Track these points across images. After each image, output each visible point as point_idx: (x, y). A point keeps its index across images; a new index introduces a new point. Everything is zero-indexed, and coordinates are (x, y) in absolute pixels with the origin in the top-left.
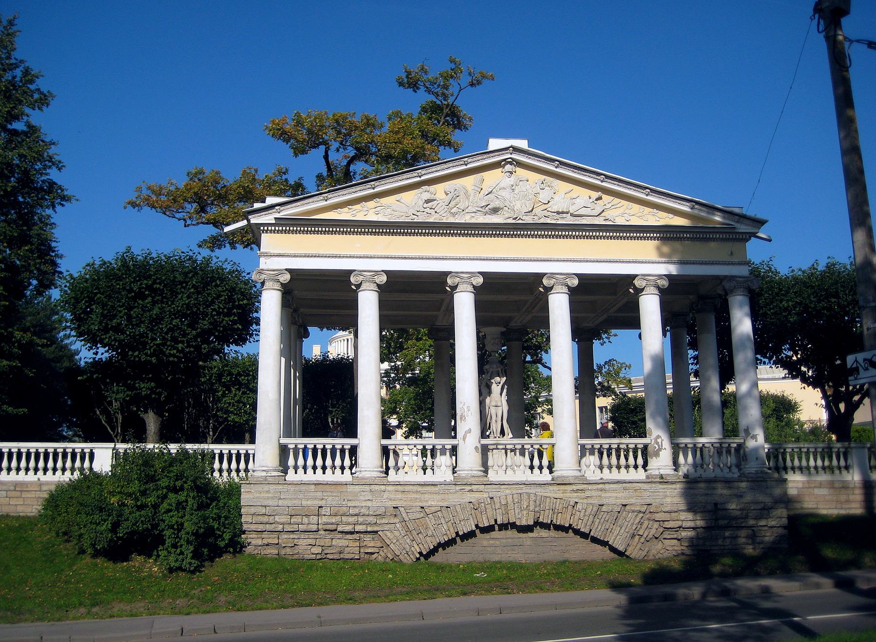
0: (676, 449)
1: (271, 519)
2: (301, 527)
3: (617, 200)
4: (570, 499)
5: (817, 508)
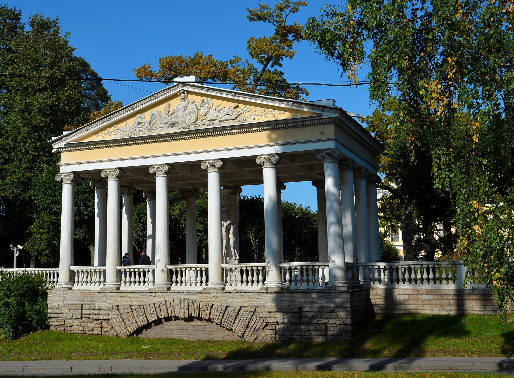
1: (60, 311)
2: (74, 316)
3: (248, 106)
4: (209, 302)
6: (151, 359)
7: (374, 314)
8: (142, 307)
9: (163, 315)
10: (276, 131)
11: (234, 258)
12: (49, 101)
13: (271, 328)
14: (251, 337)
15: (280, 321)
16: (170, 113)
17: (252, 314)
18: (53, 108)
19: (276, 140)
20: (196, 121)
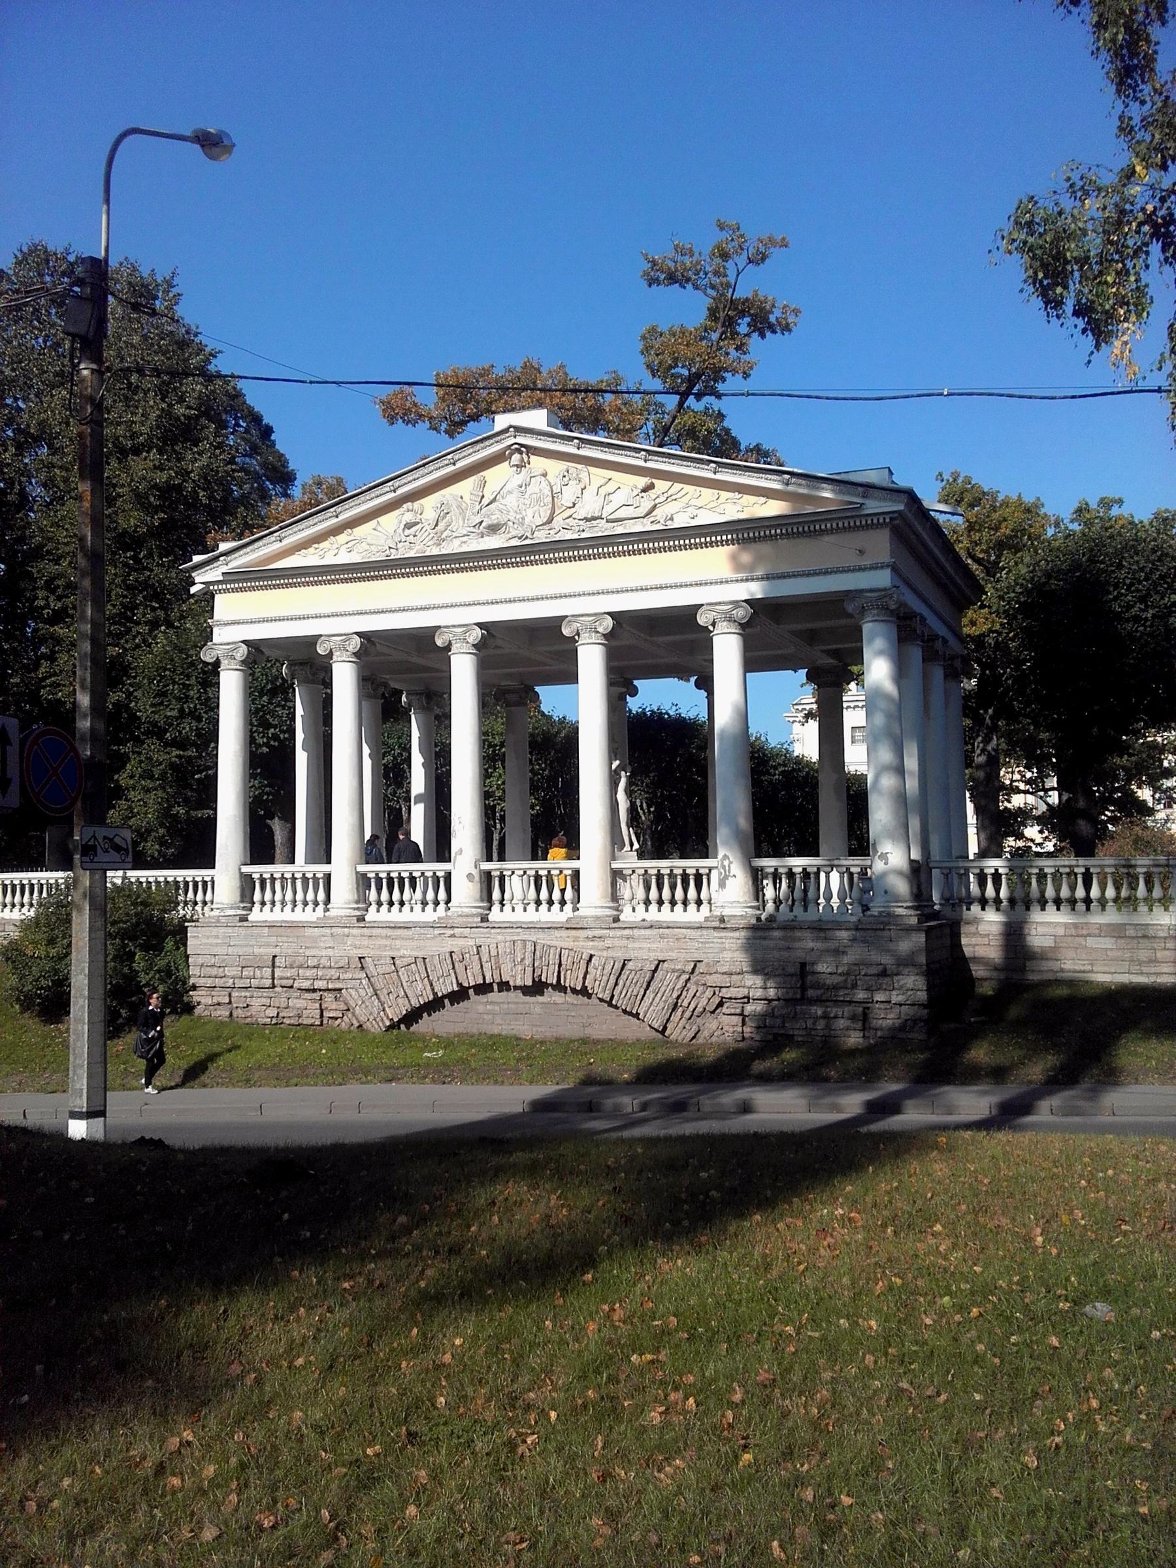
0: (757, 877)
2: (254, 982)
5: (1091, 971)
6: (449, 1082)
7: (971, 981)
8: (420, 962)
9: (471, 980)
10: (753, 545)
11: (627, 848)
12: (161, 478)
13: (733, 1011)
14: (684, 1032)
15: (759, 993)
16: (485, 501)
17: (685, 977)
18: (167, 492)
19: (751, 568)
20: (550, 521)
